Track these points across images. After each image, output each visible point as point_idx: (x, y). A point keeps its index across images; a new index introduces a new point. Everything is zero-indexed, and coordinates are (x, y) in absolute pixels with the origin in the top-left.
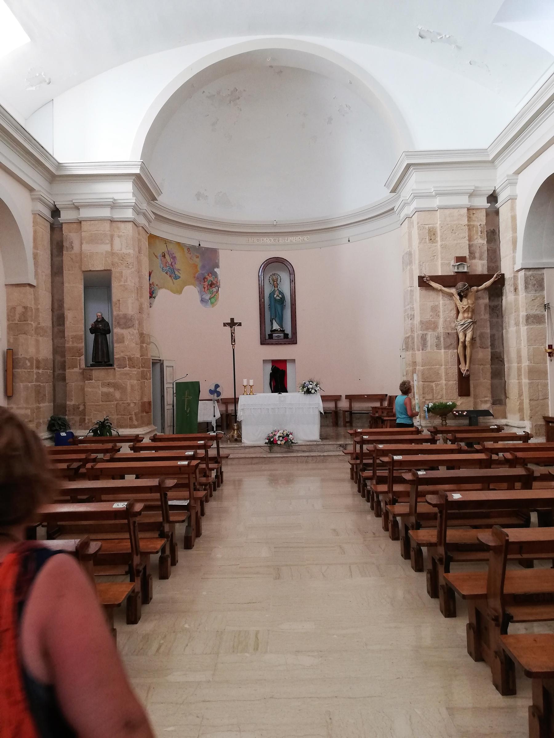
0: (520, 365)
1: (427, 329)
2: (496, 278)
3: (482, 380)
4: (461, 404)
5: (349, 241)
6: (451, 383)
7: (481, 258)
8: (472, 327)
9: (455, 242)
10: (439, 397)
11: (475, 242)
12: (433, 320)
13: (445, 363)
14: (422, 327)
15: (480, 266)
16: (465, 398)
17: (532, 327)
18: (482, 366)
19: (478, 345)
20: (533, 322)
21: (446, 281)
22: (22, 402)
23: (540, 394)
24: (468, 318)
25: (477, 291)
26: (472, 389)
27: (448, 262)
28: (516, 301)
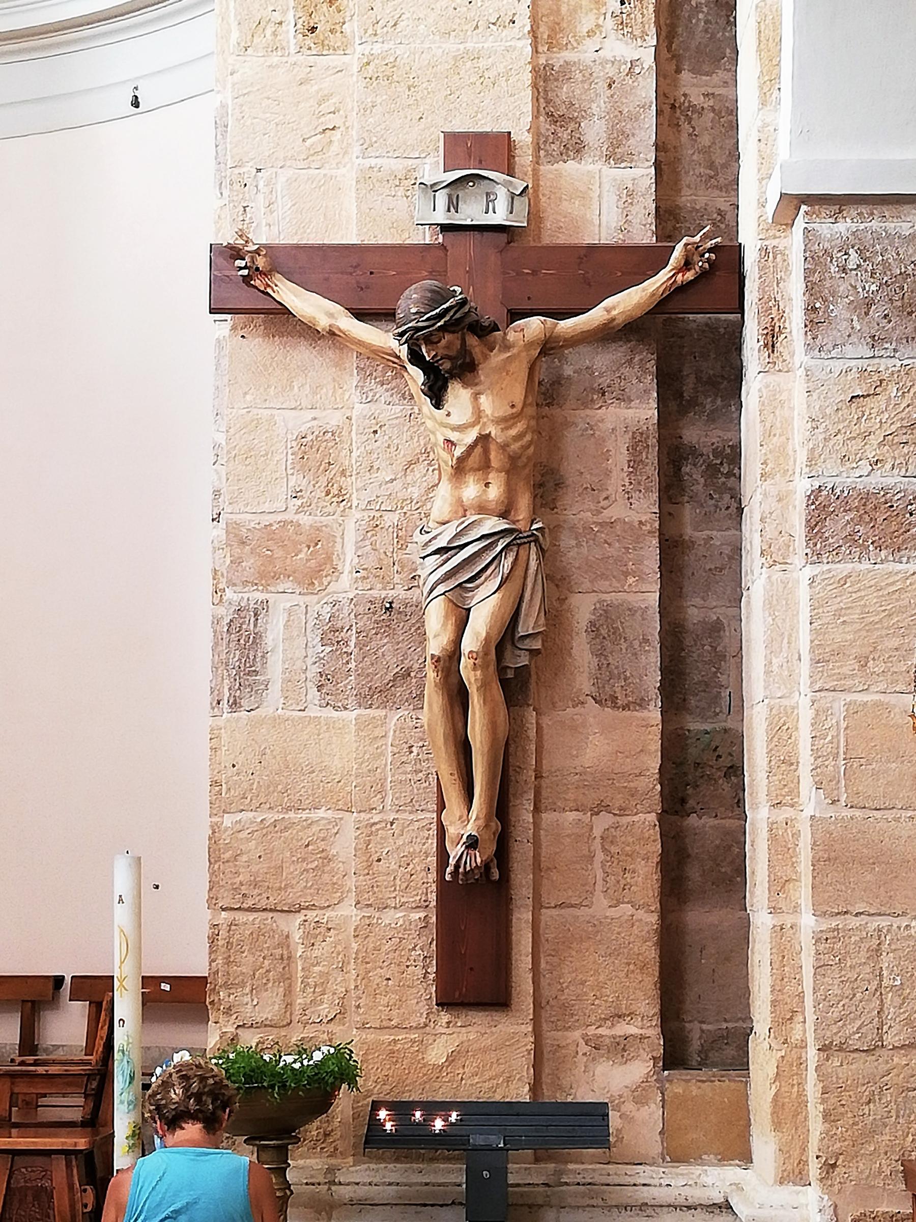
0: (786, 813)
1: (266, 577)
2: (687, 264)
3: (601, 906)
4: (452, 1059)
5: (136, 103)
6: (391, 917)
7: (616, 154)
8: (507, 563)
9: (452, 46)
10: (325, 1010)
11: (584, 53)
12: (305, 520)
13: (380, 800)
14: (236, 562)
15: (605, 198)
16: (479, 1019)
17: (843, 568)
18: (603, 822)
19: (584, 683)
20: (852, 539)
21: (361, 278)
22: (212, 1039)
23: (890, 1012)
24: (482, 509)
25: (549, 347)
26: (522, 961)
27: (398, 166)
28: (788, 410)
